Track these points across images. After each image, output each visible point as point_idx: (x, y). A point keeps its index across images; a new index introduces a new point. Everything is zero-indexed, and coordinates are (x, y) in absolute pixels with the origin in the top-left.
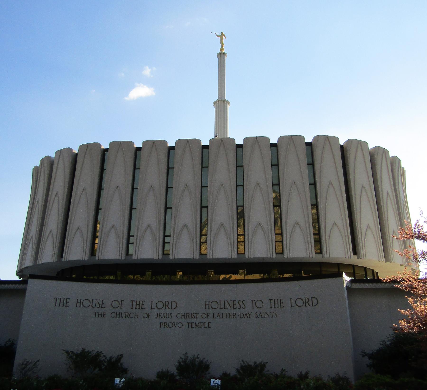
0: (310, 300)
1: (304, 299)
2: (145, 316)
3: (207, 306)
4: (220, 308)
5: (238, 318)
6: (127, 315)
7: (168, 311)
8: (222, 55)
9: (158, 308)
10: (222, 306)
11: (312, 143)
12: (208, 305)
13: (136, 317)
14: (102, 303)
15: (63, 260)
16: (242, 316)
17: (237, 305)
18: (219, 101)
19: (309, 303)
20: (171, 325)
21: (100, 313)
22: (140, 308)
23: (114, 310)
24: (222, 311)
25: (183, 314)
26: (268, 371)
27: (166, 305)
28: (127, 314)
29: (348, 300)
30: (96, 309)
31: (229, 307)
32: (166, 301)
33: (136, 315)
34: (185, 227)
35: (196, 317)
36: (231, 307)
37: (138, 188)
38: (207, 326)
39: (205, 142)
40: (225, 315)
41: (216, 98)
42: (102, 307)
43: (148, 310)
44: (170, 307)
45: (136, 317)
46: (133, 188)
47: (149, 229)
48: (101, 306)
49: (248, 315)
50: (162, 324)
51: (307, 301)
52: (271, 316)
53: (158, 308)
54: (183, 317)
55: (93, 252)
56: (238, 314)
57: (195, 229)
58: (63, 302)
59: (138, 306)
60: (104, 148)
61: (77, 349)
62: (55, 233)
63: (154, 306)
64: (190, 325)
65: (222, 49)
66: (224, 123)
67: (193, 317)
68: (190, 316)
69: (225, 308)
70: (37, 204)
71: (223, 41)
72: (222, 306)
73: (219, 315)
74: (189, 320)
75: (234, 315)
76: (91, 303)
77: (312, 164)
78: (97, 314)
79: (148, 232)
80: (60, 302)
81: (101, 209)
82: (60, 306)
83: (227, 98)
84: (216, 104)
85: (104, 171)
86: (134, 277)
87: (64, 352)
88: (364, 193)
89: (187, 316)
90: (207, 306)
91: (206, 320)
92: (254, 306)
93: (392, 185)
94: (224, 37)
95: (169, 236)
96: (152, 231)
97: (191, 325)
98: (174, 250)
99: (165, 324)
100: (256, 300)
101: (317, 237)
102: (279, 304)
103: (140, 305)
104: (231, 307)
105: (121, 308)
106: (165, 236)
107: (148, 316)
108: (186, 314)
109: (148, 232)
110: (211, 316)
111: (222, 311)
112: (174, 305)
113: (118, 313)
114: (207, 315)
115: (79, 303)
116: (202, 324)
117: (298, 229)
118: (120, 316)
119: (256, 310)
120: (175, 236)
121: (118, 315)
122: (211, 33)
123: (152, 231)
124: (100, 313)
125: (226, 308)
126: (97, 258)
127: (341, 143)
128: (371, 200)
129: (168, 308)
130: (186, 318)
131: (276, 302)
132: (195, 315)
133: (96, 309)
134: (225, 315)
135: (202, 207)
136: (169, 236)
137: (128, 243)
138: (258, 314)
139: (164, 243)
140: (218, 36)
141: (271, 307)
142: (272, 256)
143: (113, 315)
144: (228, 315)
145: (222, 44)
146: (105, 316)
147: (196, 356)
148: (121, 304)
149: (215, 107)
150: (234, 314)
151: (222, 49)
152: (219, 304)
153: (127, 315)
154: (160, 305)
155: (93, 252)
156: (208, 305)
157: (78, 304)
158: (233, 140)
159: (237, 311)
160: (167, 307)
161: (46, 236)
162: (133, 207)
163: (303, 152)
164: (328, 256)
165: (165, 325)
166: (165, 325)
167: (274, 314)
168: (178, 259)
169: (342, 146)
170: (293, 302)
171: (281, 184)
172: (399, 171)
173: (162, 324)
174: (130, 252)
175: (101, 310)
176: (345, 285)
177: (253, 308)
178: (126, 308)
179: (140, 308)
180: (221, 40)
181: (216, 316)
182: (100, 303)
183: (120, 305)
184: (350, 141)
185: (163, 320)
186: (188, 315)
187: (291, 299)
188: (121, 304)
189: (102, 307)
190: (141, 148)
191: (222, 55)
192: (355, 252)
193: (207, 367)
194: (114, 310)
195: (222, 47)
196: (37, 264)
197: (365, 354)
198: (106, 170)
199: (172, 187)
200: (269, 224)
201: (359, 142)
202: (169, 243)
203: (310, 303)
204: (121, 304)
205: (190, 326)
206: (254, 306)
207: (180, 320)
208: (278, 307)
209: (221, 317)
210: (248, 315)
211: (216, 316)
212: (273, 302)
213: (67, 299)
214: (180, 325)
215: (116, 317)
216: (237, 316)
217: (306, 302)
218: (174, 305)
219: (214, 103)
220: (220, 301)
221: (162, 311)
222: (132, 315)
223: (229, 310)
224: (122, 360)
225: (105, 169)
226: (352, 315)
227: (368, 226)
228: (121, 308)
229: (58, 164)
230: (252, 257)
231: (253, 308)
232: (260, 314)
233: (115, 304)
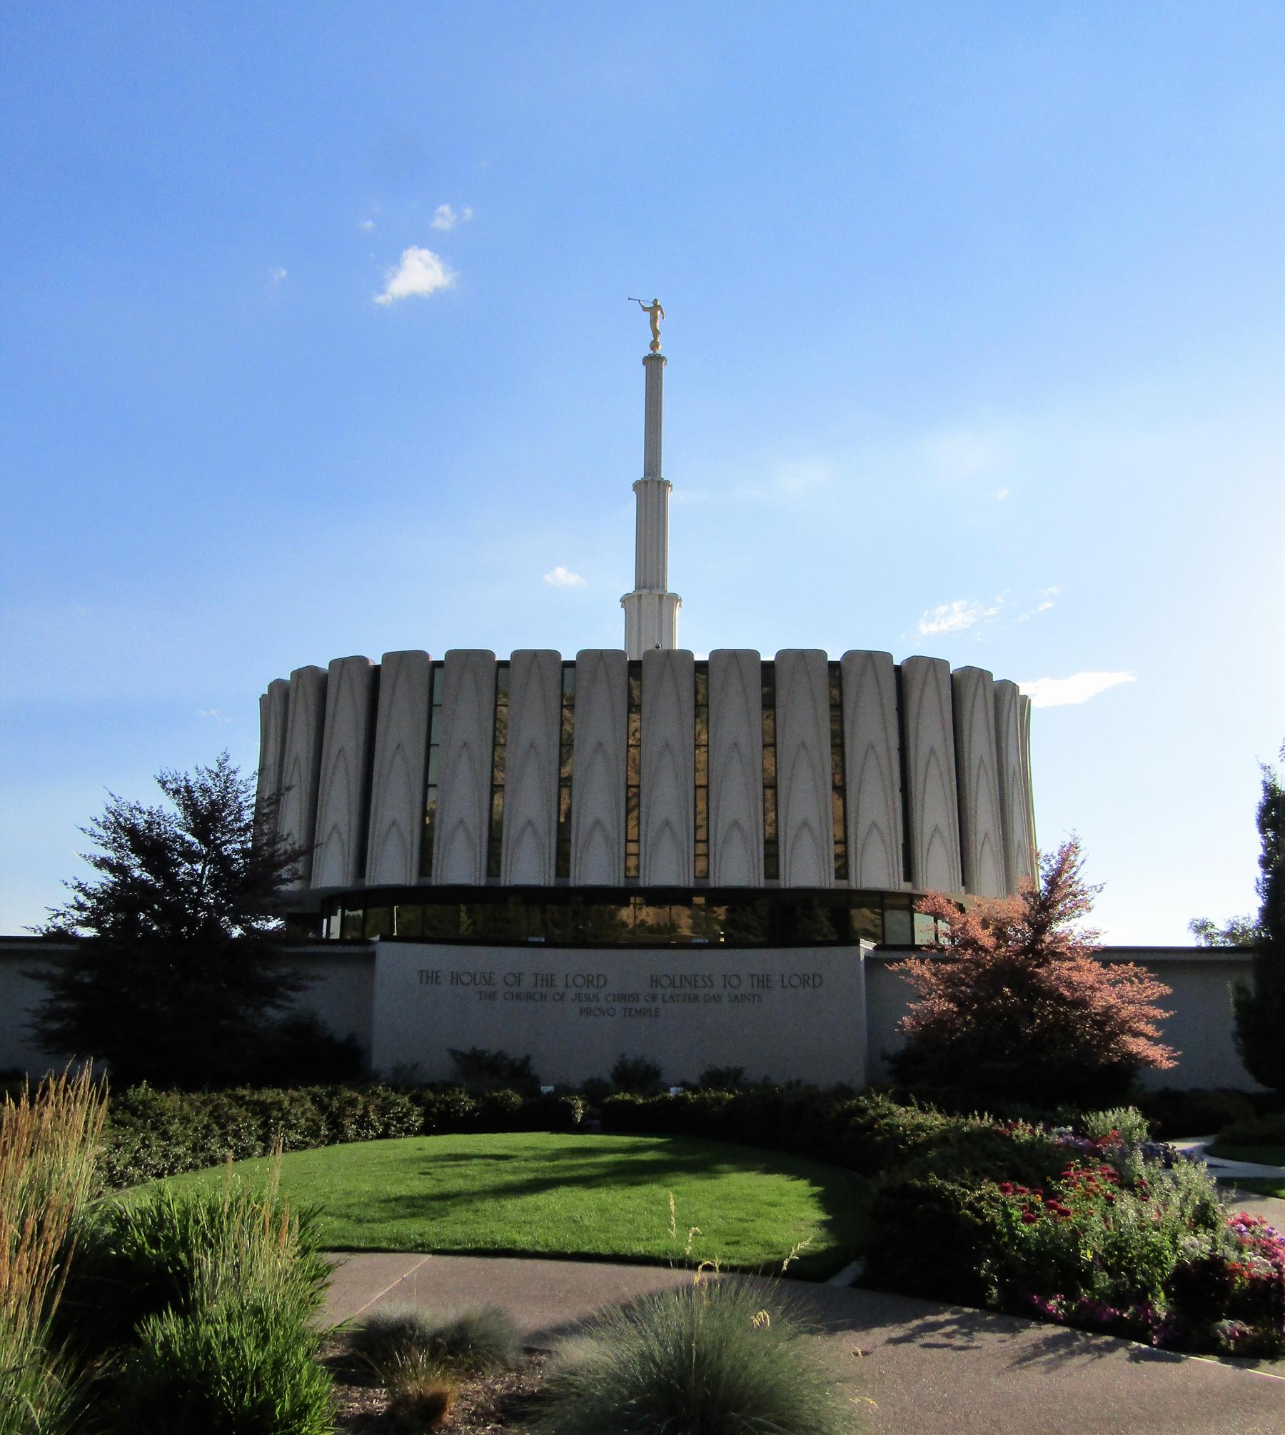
2: (557, 997)
6: (530, 997)
7: (592, 991)
8: (654, 363)
10: (678, 983)
11: (842, 664)
12: (655, 981)
17: (701, 983)
18: (646, 482)
26: (746, 1079)
27: (588, 981)
29: (866, 976)
30: (483, 988)
31: (687, 985)
33: (544, 997)
38: (653, 1014)
41: (640, 475)
48: (489, 981)
49: (717, 999)
61: (465, 1048)
62: (344, 830)
63: (570, 982)
65: (654, 345)
66: (658, 552)
70: (294, 766)
71: (658, 324)
72: (678, 983)
73: (672, 997)
75: (696, 999)
76: (474, 977)
77: (837, 707)
83: (665, 475)
88: (933, 764)
89: (622, 998)
92: (727, 983)
93: (993, 739)
94: (659, 312)
96: (535, 832)
100: (730, 974)
101: (840, 849)
103: (549, 980)
107: (562, 997)
111: (678, 991)
115: (456, 979)
117: (806, 836)
119: (729, 989)
121: (518, 997)
122: (629, 299)
123: (535, 832)
127: (897, 662)
128: (946, 779)
140: (645, 309)
145: (656, 333)
149: (636, 493)
151: (654, 345)
153: (530, 997)
154: (579, 981)
158: (687, 654)
159: (701, 992)
160: (590, 984)
163: (821, 682)
165: (587, 1012)
166: (587, 1012)
169: (898, 669)
170: (786, 980)
171: (779, 746)
172: (1012, 710)
176: (862, 958)
178: (527, 985)
180: (654, 321)
181: (667, 998)
182: (487, 976)
185: (585, 1005)
188: (518, 978)
191: (654, 363)
192: (909, 875)
193: (657, 1074)
195: (656, 338)
196: (312, 887)
197: (885, 1057)
204: (518, 978)
206: (727, 983)
210: (717, 999)
211: (667, 998)
217: (805, 981)
218: (601, 983)
221: (584, 991)
223: (688, 990)
224: (531, 1063)
226: (870, 1001)
227: (936, 829)
233: (511, 979)
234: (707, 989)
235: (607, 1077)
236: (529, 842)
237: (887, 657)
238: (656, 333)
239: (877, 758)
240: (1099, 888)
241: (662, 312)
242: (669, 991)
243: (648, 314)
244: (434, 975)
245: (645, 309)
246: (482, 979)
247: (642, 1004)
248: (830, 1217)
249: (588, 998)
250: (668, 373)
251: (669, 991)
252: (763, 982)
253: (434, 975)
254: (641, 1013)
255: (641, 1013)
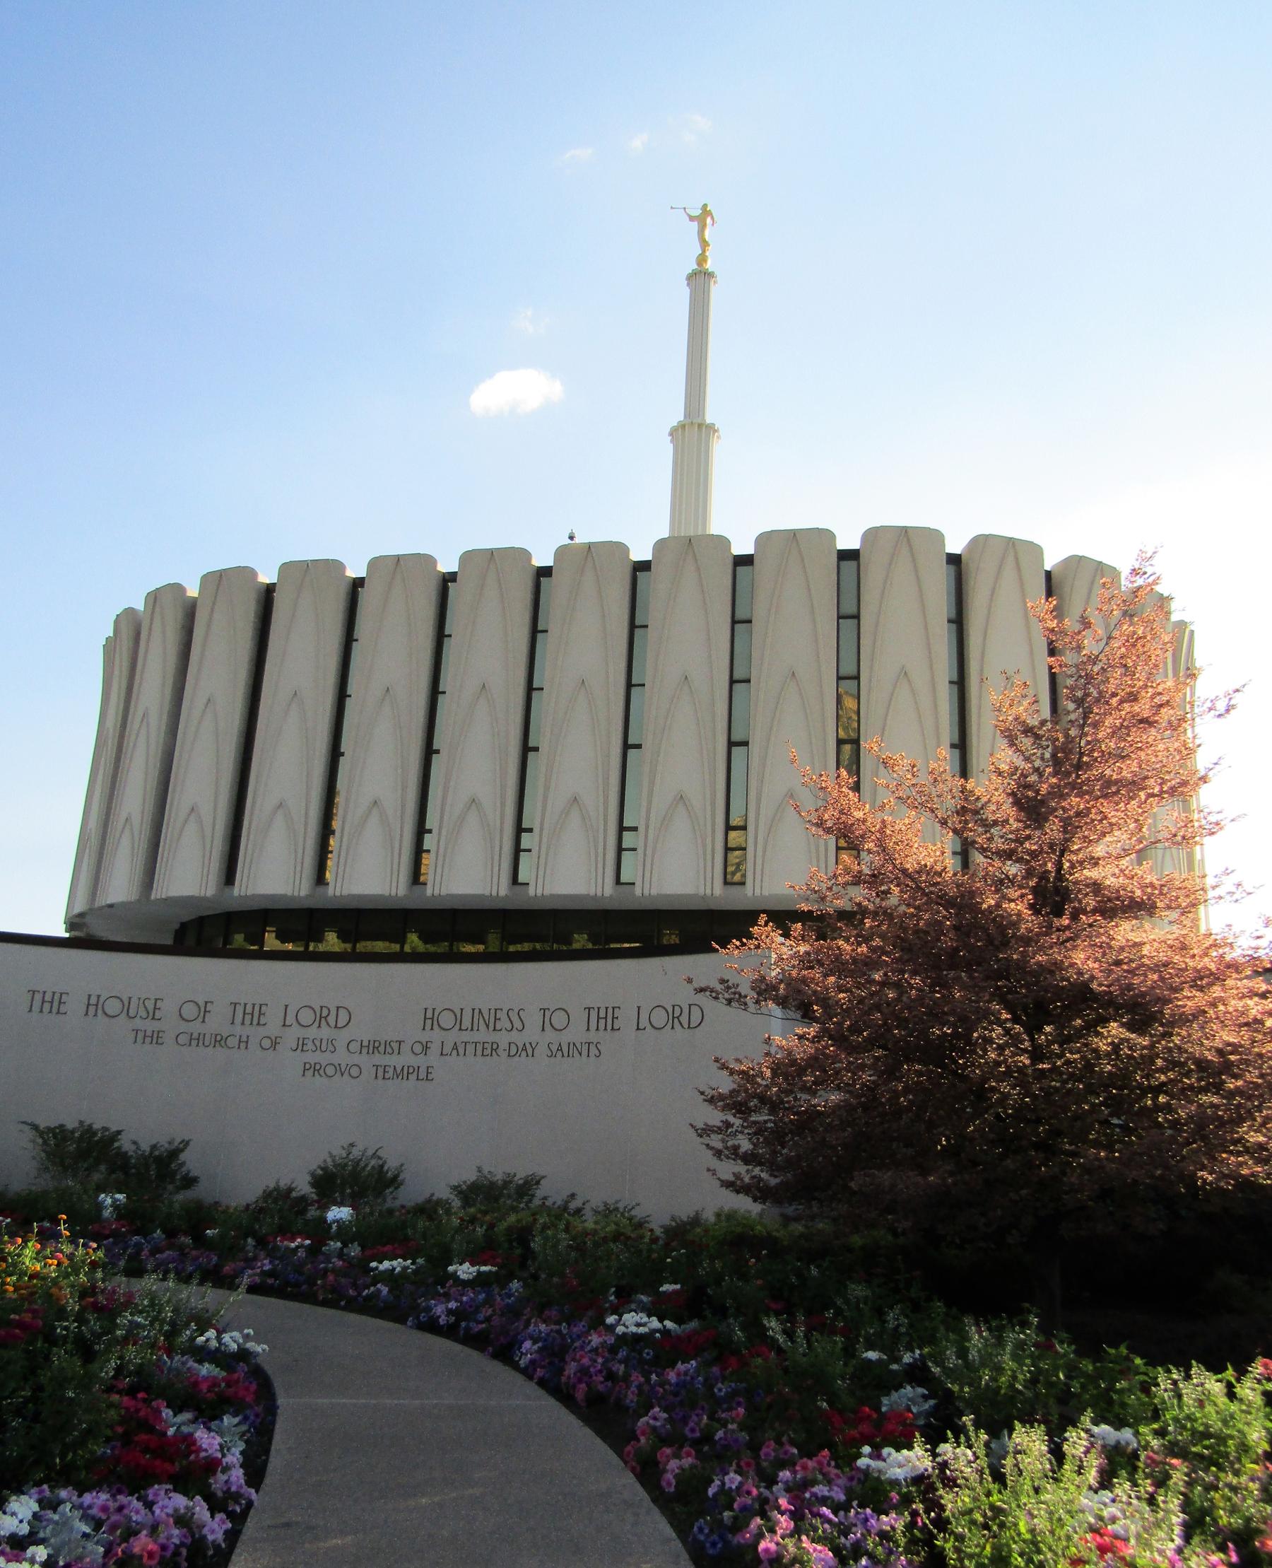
0: (686, 1011)
1: (670, 1010)
2: (266, 1043)
3: (429, 1022)
4: (460, 1029)
5: (504, 1055)
6: (219, 1041)
7: (325, 1032)
8: (700, 279)
9: (299, 1024)
10: (466, 1023)
12: (430, 1019)
13: (243, 1045)
14: (155, 1008)
15: (153, 897)
16: (513, 1051)
19: (681, 1018)
20: (330, 1071)
21: (149, 1033)
22: (255, 1022)
23: (183, 1027)
24: (466, 1036)
25: (365, 1043)
28: (219, 1038)
30: (138, 1023)
32: (322, 1007)
33: (244, 1043)
34: (474, 807)
35: (396, 1051)
36: (488, 1026)
37: (644, 685)
38: (422, 1075)
39: (641, 552)
40: (470, 1048)
42: (153, 1018)
43: (273, 1028)
44: (332, 1023)
45: (243, 1045)
46: (530, 689)
47: (375, 811)
49: (527, 1050)
50: (307, 1066)
51: (677, 1014)
52: (585, 1052)
53: (299, 1024)
54: (365, 1050)
55: (416, 877)
56: (503, 1045)
57: (498, 813)
58: (606, 1018)
59: (248, 1018)
60: (268, 582)
61: (46, 1121)
62: (136, 821)
63: (290, 1019)
64: (381, 1070)
65: (702, 259)
67: (389, 1049)
68: (383, 1046)
69: (472, 1030)
72: (466, 1023)
73: (455, 1047)
74: (378, 1059)
75: (495, 1048)
77: (849, 617)
78: (140, 1035)
79: (374, 820)
80: (43, 1001)
81: (437, 752)
82: (41, 1011)
84: (677, 433)
85: (446, 639)
86: (354, 947)
87: (27, 1128)
89: (373, 1047)
90: (429, 1022)
91: (420, 1061)
94: (709, 220)
95: (635, 829)
97: (382, 1072)
98: (439, 870)
99: (317, 1067)
102: (56, 1004)
103: (255, 1014)
104: (488, 1026)
105: (203, 1021)
106: (622, 829)
107: (274, 1044)
108: (372, 1043)
109: (374, 820)
110: (435, 1049)
111: (466, 1036)
112: (343, 1017)
113: (195, 1035)
114: (426, 1048)
115: (94, 1006)
116: (411, 1071)
118: (201, 1042)
119: (550, 1035)
120: (444, 832)
124: (149, 1033)
125: (475, 1028)
126: (429, 892)
129: (328, 1024)
130: (371, 1051)
131: (46, 999)
132: (395, 1045)
133: (137, 1020)
134: (470, 1048)
135: (731, 744)
136: (635, 829)
137: (517, 850)
138: (554, 1048)
139: (620, 850)
140: (692, 219)
141: (588, 1029)
142: (494, 893)
143: (182, 1039)
144: (480, 1048)
145: (704, 244)
146: (160, 1040)
147: (370, 1153)
148: (205, 1011)
150: (495, 1047)
151: (702, 259)
152: (459, 1020)
153: (219, 1041)
154: (307, 1017)
155: (416, 877)
156: (430, 1019)
157: (92, 1009)
158: (723, 542)
159: (503, 1039)
161: (120, 827)
162: (531, 745)
164: (758, 892)
165: (316, 1069)
166: (316, 1069)
167: (593, 1051)
168: (552, 896)
169: (954, 560)
173: (307, 1066)
174: (522, 878)
175: (150, 1026)
177: (543, 1030)
178: (217, 1022)
179: (255, 1022)
181: (447, 1050)
182: (150, 1005)
183: (202, 1014)
184: (981, 543)
185: (312, 1058)
186: (376, 1045)
187: (639, 1008)
188: (204, 1011)
189: (153, 1018)
190: (551, 568)
191: (700, 279)
194: (183, 1027)
195: (704, 251)
198: (450, 636)
199: (644, 685)
200: (708, 796)
201: (1011, 543)
202: (634, 850)
203: (684, 1019)
204: (204, 1011)
205: (380, 1074)
207: (356, 1059)
208: (605, 1029)
209: (461, 1051)
210: (527, 1050)
211: (447, 1050)
212: (38, 997)
213: (61, 994)
214: (355, 1072)
215: (190, 1044)
216: (500, 1051)
218: (343, 1017)
219: (671, 434)
220: (130, 998)
221: (312, 1032)
222: (232, 1042)
223: (483, 1035)
225: (355, 637)
228: (203, 1021)
229: (150, 629)
230: (654, 892)
231: (543, 1030)
232: (560, 1049)
233: (189, 1011)
234: (514, 1032)
235: (304, 1187)
236: (373, 832)
237: (935, 537)
238: (704, 244)
239: (913, 692)
240: (1221, 706)
241: (713, 218)
242: (453, 1037)
243: (695, 225)
244: (57, 998)
245: (692, 219)
246: (142, 1009)
247: (405, 1059)
248: (1194, 1363)
249: (318, 1048)
250: (717, 293)
251: (453, 1037)
252: (606, 1018)
253: (57, 998)
254: (404, 1073)
255: (404, 1073)
